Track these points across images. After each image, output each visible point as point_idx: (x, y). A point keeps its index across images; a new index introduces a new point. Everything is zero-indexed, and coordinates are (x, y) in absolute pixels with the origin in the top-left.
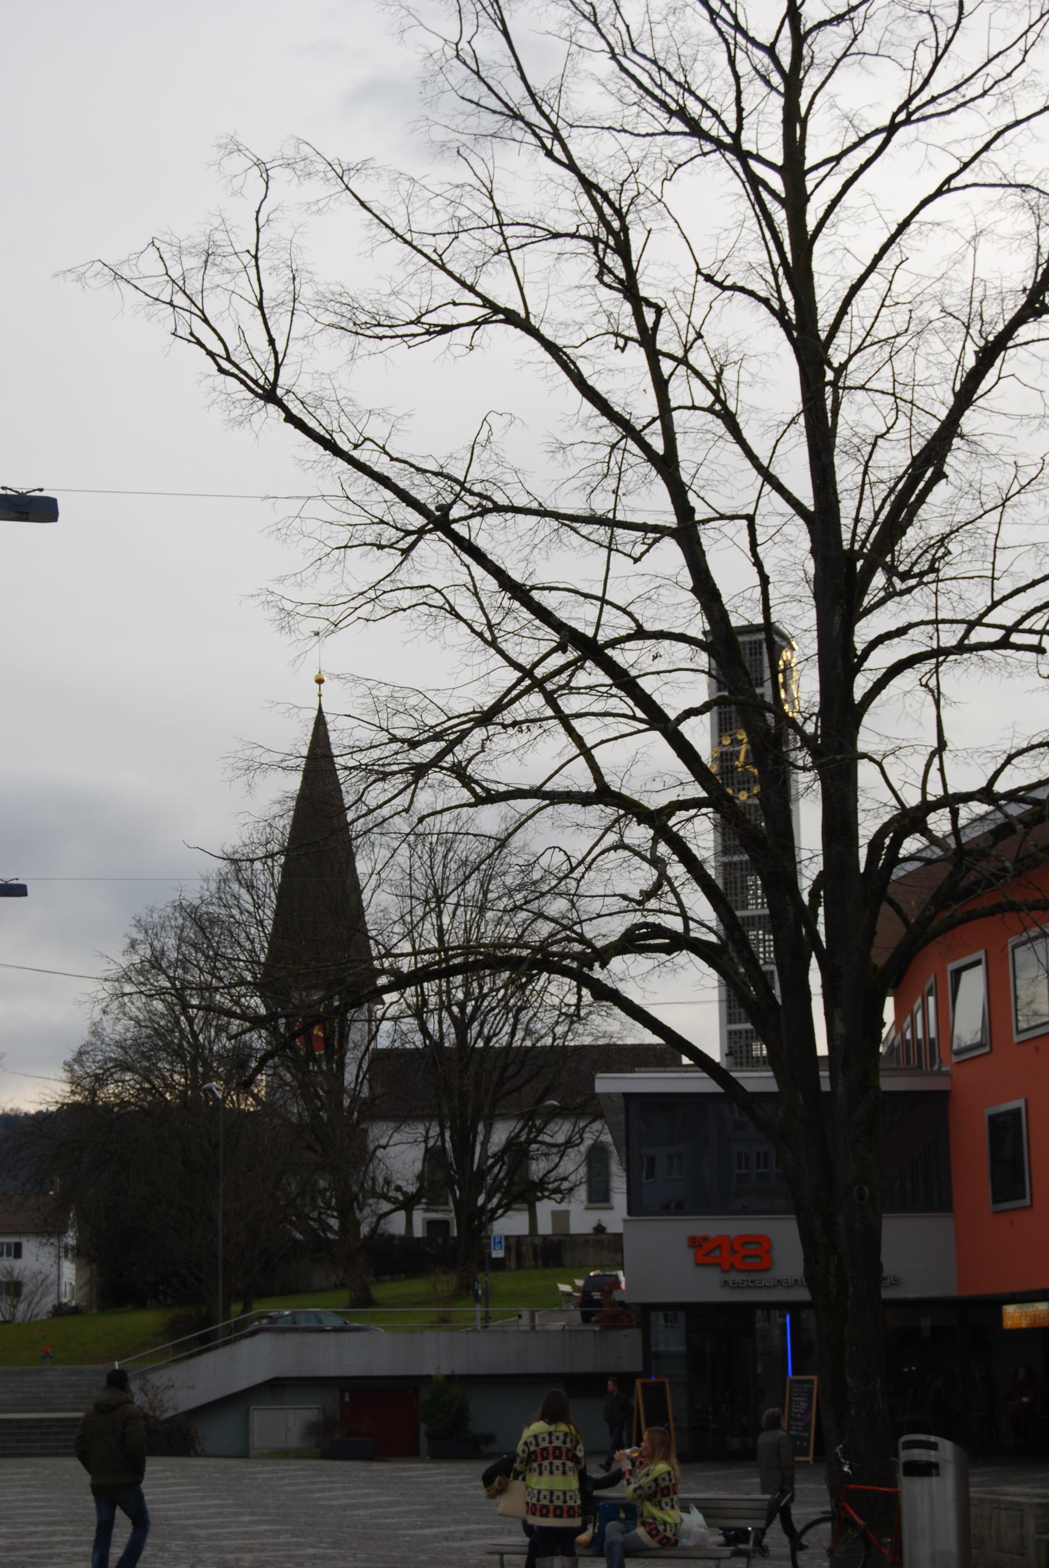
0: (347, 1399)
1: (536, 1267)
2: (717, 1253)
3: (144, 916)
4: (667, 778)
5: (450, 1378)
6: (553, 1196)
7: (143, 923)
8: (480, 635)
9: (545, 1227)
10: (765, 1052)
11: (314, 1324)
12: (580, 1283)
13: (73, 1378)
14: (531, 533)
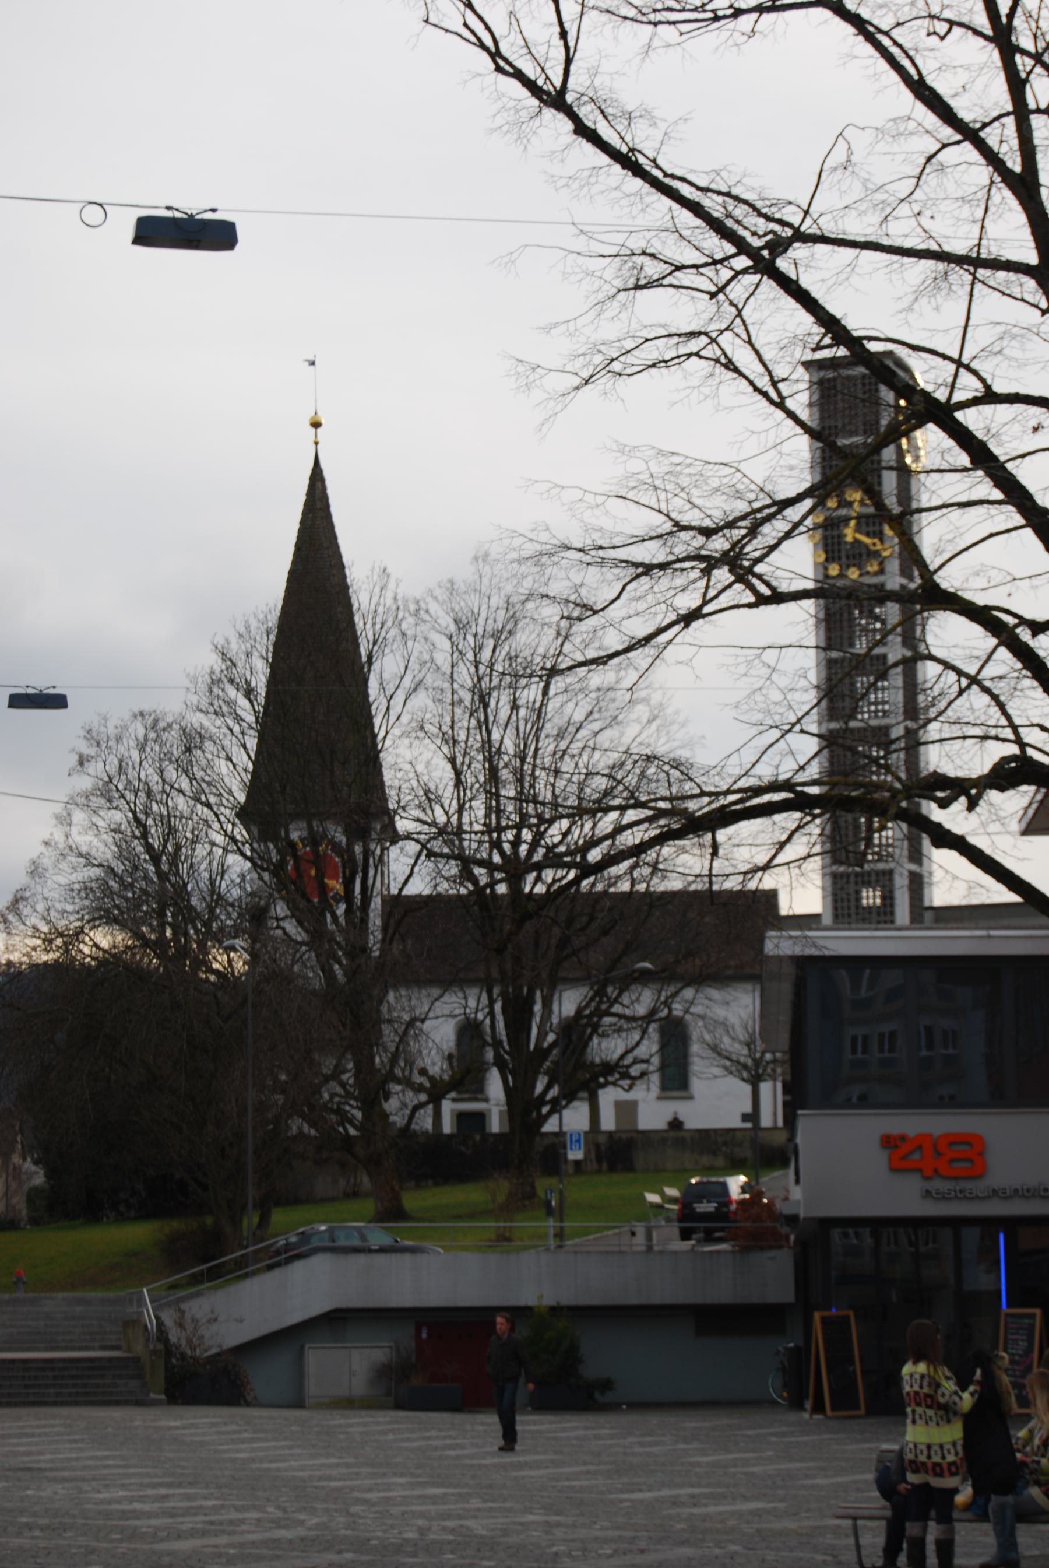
0: (424, 1335)
1: (599, 1171)
2: (916, 1156)
3: (95, 726)
4: (993, 573)
5: (556, 1311)
6: (621, 1082)
7: (94, 734)
8: (765, 395)
9: (608, 1122)
10: (878, 901)
11: (356, 1242)
12: (672, 1192)
13: (78, 1309)
14: (849, 269)
